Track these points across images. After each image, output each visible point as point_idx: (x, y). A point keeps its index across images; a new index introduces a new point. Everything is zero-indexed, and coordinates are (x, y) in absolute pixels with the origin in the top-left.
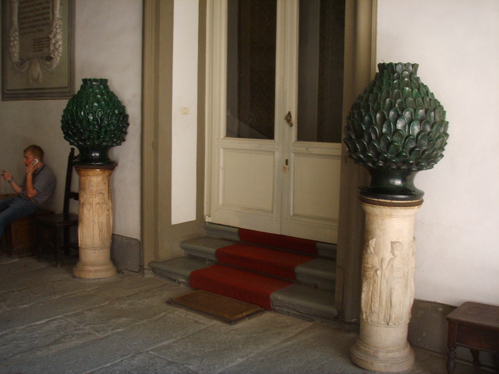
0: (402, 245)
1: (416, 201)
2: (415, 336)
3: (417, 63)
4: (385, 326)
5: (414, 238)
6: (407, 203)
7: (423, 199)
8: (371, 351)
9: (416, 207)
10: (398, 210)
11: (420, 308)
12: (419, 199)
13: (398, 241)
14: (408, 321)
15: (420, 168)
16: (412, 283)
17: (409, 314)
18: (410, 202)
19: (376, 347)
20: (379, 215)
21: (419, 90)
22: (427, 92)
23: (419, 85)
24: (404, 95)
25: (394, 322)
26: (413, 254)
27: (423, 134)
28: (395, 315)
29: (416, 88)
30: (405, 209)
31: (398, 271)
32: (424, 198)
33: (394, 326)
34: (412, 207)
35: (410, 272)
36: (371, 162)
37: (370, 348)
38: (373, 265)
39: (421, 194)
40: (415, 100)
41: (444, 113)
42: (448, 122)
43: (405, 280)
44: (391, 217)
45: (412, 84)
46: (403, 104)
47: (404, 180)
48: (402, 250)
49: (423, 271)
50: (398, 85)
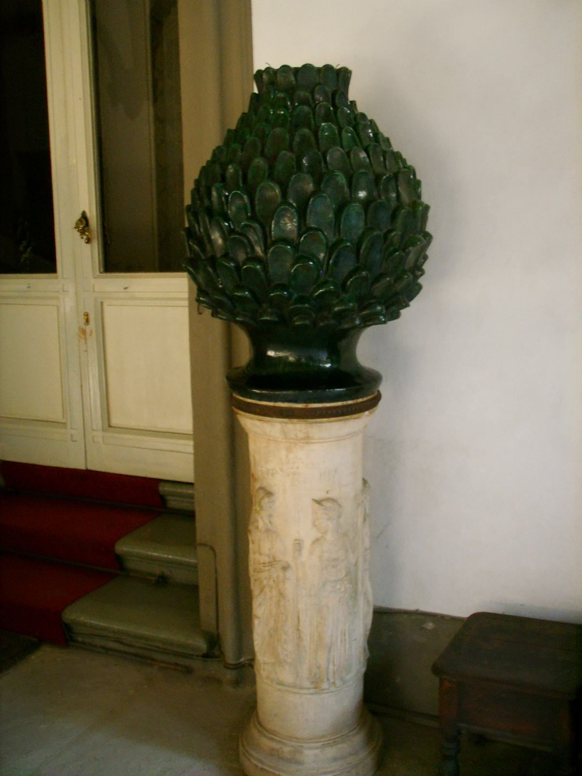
0: (340, 506)
1: (365, 399)
2: (382, 698)
3: (350, 68)
4: (312, 691)
5: (365, 482)
6: (343, 406)
7: (379, 391)
8: (286, 749)
9: (367, 413)
10: (324, 425)
11: (389, 631)
12: (372, 394)
13: (329, 496)
14: (363, 670)
15: (370, 320)
16: (368, 583)
17: (365, 650)
18: (350, 402)
19: (296, 738)
20: (279, 440)
21: (355, 128)
22: (376, 133)
23: (355, 118)
24: (320, 141)
25: (332, 681)
26: (365, 520)
27: (278, 295)
28: (334, 665)
29: (349, 124)
30: (340, 420)
31: (333, 566)
32: (383, 388)
33: (333, 688)
34: (356, 416)
35: (361, 560)
36: (190, 227)
37: (283, 743)
38: (274, 558)
39: (374, 379)
40: (348, 154)
41: (417, 184)
42: (427, 208)
43: (351, 583)
44: (307, 443)
45: (339, 115)
46: (320, 162)
47: (334, 353)
48: (339, 517)
49: (387, 547)
50: (310, 110)
